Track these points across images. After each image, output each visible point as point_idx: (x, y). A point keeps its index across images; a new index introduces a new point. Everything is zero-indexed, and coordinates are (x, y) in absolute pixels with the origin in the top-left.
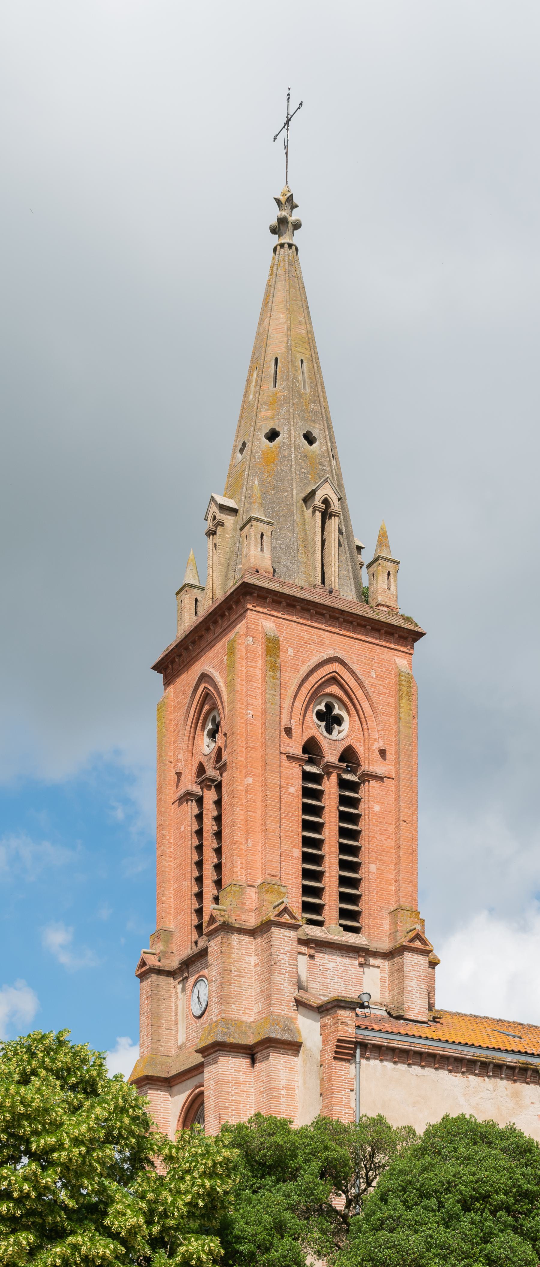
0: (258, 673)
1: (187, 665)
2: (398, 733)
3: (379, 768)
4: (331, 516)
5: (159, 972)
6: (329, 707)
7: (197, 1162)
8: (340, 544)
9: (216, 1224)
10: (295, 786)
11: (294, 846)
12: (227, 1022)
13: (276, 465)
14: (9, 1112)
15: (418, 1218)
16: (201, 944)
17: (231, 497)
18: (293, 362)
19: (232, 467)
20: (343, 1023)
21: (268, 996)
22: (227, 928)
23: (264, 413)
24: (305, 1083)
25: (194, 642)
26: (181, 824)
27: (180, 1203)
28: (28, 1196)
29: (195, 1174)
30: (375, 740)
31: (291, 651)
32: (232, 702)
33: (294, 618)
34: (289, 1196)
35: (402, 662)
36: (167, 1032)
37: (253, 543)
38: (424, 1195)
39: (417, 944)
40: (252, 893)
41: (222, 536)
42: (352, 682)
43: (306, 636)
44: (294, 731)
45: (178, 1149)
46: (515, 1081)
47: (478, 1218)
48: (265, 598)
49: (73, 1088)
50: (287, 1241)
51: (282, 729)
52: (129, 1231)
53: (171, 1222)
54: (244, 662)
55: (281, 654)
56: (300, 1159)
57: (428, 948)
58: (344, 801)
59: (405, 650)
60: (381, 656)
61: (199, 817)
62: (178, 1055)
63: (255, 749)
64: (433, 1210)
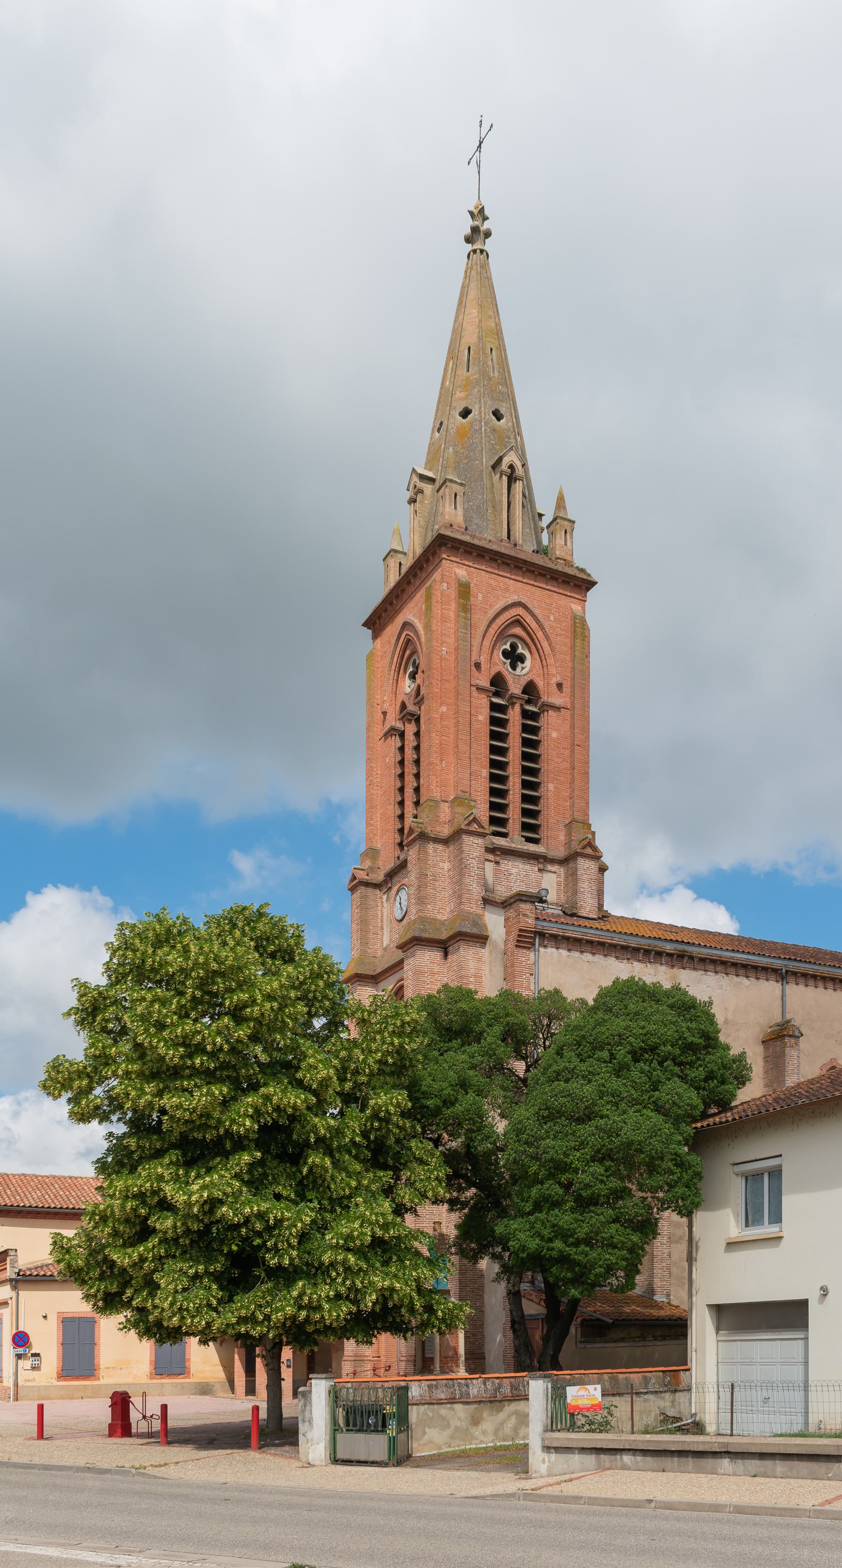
0: (452, 615)
1: (391, 618)
2: (573, 669)
3: (557, 699)
4: (516, 479)
5: (367, 884)
6: (514, 647)
7: (387, 1023)
8: (523, 506)
9: (405, 1080)
10: (483, 716)
11: (483, 767)
12: (423, 920)
13: (469, 438)
14: (203, 969)
15: (591, 1069)
16: (402, 858)
17: (430, 470)
18: (484, 350)
19: (431, 445)
20: (524, 915)
21: (459, 896)
22: (424, 837)
23: (459, 394)
24: (491, 971)
25: (397, 597)
26: (386, 756)
27: (371, 1061)
28: (221, 1049)
29: (386, 1034)
30: (553, 675)
31: (480, 596)
32: (429, 640)
33: (483, 568)
34: (473, 1057)
35: (576, 607)
36: (374, 936)
37: (447, 501)
38: (597, 1046)
39: (589, 851)
40: (445, 807)
41: (422, 502)
42: (534, 625)
43: (494, 583)
44: (483, 666)
45: (370, 1013)
46: (673, 966)
47: (647, 1068)
48: (458, 549)
49: (273, 956)
50: (471, 1096)
51: (473, 664)
52: (321, 1084)
53: (363, 1079)
54: (439, 606)
55: (472, 598)
56: (483, 1024)
57: (598, 854)
58: (525, 728)
59: (579, 597)
60: (560, 603)
61: (402, 749)
62: (383, 956)
63: (448, 681)
64: (605, 1062)
